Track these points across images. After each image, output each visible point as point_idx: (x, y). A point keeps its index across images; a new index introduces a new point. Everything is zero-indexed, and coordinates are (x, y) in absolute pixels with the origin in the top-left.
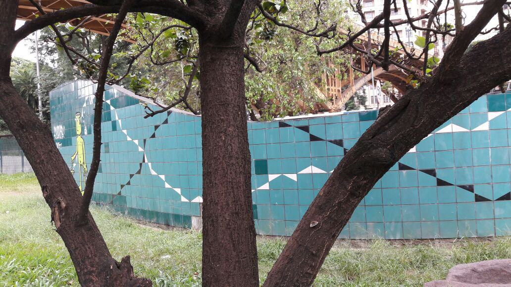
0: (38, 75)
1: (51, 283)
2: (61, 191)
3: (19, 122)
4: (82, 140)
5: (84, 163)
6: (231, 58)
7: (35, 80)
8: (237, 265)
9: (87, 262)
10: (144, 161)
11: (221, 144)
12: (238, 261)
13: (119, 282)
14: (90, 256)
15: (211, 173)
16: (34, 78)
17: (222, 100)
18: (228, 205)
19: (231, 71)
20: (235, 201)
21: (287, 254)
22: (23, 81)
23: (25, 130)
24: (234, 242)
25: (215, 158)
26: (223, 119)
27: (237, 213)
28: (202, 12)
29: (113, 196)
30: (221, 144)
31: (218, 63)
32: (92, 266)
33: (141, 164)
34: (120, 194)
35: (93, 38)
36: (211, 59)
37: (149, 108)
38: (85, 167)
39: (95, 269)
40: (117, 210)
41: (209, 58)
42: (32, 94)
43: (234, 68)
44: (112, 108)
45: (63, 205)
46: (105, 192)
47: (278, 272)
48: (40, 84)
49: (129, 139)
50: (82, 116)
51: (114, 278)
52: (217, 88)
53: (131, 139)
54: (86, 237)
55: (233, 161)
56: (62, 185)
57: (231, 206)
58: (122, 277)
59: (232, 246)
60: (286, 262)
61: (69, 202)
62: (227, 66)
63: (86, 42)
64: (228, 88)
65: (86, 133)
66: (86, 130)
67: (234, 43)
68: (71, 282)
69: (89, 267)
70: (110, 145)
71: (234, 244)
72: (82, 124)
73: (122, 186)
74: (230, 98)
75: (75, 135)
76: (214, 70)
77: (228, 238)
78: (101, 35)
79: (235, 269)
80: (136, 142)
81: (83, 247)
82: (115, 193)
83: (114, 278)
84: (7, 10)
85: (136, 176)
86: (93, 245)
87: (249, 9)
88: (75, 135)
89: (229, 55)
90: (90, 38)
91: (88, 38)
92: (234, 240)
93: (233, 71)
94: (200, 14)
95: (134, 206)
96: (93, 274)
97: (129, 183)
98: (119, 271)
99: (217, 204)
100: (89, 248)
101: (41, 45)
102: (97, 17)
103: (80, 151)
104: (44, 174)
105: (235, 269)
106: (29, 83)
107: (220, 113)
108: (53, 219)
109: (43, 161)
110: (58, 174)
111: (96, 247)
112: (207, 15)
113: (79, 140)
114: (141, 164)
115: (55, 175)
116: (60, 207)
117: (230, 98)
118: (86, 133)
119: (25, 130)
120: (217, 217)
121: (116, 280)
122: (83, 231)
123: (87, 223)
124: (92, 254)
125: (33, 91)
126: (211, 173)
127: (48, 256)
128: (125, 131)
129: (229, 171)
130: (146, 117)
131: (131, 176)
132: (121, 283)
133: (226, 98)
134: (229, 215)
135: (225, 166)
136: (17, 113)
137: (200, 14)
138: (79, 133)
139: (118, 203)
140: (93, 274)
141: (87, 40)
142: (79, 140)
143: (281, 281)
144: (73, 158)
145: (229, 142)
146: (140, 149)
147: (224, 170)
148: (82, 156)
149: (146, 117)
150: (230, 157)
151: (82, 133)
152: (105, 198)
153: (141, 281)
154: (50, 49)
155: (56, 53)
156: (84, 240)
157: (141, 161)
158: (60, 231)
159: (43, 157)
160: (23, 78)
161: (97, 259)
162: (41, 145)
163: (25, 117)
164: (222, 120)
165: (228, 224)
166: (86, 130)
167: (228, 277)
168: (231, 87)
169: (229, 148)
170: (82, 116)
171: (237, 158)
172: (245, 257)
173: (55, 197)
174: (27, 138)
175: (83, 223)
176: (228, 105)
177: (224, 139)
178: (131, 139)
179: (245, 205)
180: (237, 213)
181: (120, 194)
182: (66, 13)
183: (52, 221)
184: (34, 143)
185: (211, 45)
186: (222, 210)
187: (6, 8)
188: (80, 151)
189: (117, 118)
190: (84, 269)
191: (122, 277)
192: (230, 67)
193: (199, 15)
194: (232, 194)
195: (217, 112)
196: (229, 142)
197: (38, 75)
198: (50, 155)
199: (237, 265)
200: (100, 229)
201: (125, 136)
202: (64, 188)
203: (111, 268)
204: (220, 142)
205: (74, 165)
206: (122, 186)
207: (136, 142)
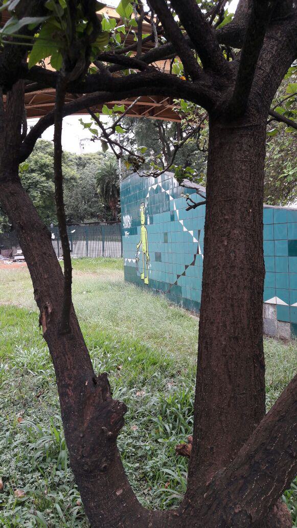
0: (120, 166)
1: (102, 365)
2: (49, 295)
3: (19, 223)
4: (145, 230)
5: (146, 251)
6: (245, 140)
7: (117, 171)
8: (233, 401)
9: (65, 374)
10: (198, 253)
11: (222, 250)
12: (233, 397)
13: (91, 401)
14: (69, 368)
15: (208, 284)
16: (116, 170)
17: (229, 195)
18: (225, 326)
19: (243, 157)
20: (234, 323)
21: (278, 409)
22: (107, 172)
23: (24, 231)
24: (230, 374)
25: (214, 267)
26: (227, 219)
27: (236, 338)
28: (210, 87)
29: (170, 284)
30: (222, 250)
31: (228, 148)
32: (70, 379)
33: (195, 256)
34: (176, 283)
35: (169, 126)
36: (221, 144)
37: (190, 200)
38: (148, 256)
39: (72, 382)
40: (173, 300)
41: (218, 143)
42: (114, 185)
43: (247, 153)
44: (171, 198)
45: (50, 310)
46: (163, 280)
47: (266, 429)
48: (121, 175)
49: (185, 229)
50: (146, 206)
51: (87, 396)
52: (223, 180)
53: (189, 231)
54: (67, 346)
55: (236, 272)
56: (50, 289)
57: (228, 328)
58: (95, 397)
59: (227, 377)
60: (277, 418)
61: (55, 307)
62: (238, 151)
63: (162, 131)
64: (237, 179)
65: (148, 223)
66: (148, 220)
67: (249, 121)
68: (120, 367)
69: (67, 379)
70: (169, 235)
71: (230, 376)
72: (145, 214)
73: (178, 276)
74: (238, 192)
75: (140, 224)
76: (221, 157)
77: (223, 367)
78: (177, 123)
79: (229, 406)
80: (191, 232)
81: (63, 357)
82: (172, 283)
83: (87, 396)
84: (13, 109)
85: (191, 267)
86: (73, 356)
87: (276, 74)
88: (140, 224)
89: (241, 136)
90: (167, 127)
91: (164, 127)
92: (230, 370)
93: (246, 157)
94: (206, 89)
95: (189, 297)
96: (70, 388)
97: (184, 274)
98: (93, 389)
99: (212, 323)
100: (69, 359)
101: (123, 137)
102: (156, 107)
103: (144, 241)
104: (36, 277)
105: (229, 406)
106: (112, 174)
107: (225, 212)
108: (41, 323)
109: (36, 263)
110: (48, 278)
111: (76, 359)
112: (217, 90)
113: (143, 229)
114: (195, 256)
115: (45, 279)
116: (47, 312)
117: (238, 192)
118: (148, 223)
119: (24, 231)
120: (211, 339)
121: (89, 398)
122: (65, 339)
123: (70, 332)
124: (71, 365)
125: (116, 182)
126: (208, 284)
127: (106, 338)
128: (181, 222)
129: (229, 285)
130: (187, 210)
131: (186, 267)
132: (94, 403)
133: (233, 193)
134: (225, 339)
135: (225, 277)
136: (19, 213)
137: (206, 89)
138: (143, 222)
139: (174, 293)
140: (70, 388)
141: (163, 129)
142: (143, 229)
143: (268, 441)
144: (138, 246)
145: (233, 248)
146: (195, 240)
147: (223, 283)
148: (145, 244)
149: (187, 210)
150: (233, 267)
151: (146, 223)
152: (164, 287)
153: (113, 404)
154: (130, 140)
155: (136, 144)
156: (65, 349)
157: (195, 253)
158: (45, 336)
159: (36, 259)
160: (108, 169)
161: (75, 371)
162: (36, 247)
163: (26, 218)
164: (226, 220)
165: (224, 350)
166: (148, 220)
167: (221, 414)
168: (241, 178)
169: (232, 255)
170: (146, 206)
171: (242, 269)
172: (244, 394)
173: (43, 302)
174: (25, 240)
175: (65, 331)
176: (235, 200)
177: (226, 243)
178: (189, 231)
179: (248, 328)
180: (236, 338)
181: (176, 283)
182: (71, 105)
183: (40, 326)
184: (31, 244)
185: (221, 126)
186: (218, 332)
187: (12, 107)
188: (144, 241)
189: (175, 209)
190: (62, 380)
191: (95, 397)
192: (242, 152)
193: (205, 90)
194: (231, 314)
195: (221, 210)
196: (233, 248)
197: (120, 166)
198: (43, 258)
199: (233, 401)
200: (85, 338)
201: (181, 226)
202: (52, 292)
203: (86, 384)
204: (221, 247)
205: (139, 253)
206: (178, 276)
207: (191, 232)
